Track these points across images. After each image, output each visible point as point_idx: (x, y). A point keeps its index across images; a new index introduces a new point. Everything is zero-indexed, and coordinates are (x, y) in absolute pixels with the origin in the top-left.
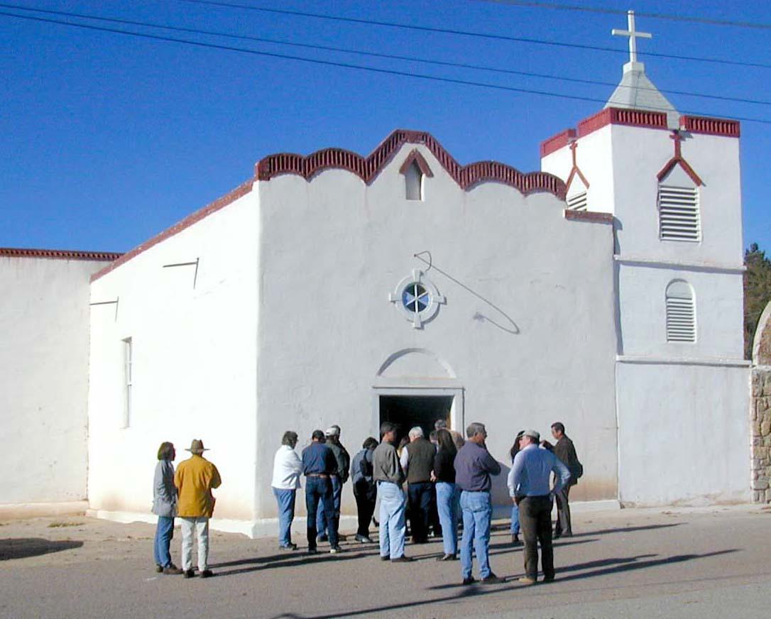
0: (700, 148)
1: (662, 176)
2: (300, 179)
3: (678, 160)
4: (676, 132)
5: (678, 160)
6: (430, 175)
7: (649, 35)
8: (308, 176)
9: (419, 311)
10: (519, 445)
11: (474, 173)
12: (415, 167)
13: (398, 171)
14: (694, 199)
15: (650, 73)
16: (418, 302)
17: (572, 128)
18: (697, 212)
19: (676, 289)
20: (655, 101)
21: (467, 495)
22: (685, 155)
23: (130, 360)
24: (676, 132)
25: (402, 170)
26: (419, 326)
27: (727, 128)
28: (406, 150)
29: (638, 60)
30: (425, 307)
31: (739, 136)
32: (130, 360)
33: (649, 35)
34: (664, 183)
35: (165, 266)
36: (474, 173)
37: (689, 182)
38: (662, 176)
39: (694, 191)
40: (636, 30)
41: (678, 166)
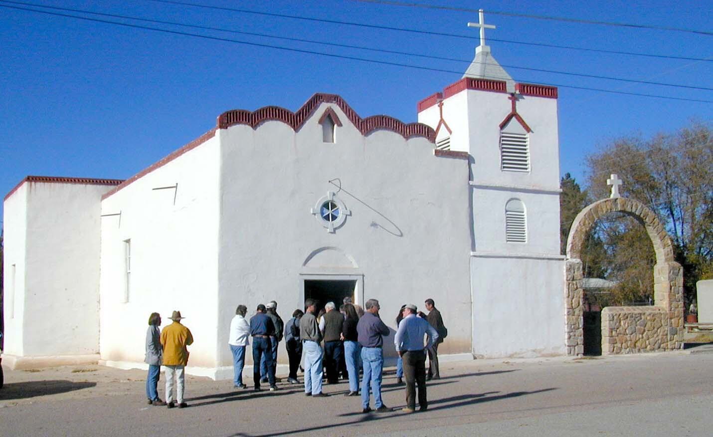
0: (529, 106)
1: (503, 126)
2: (248, 128)
3: (514, 114)
4: (512, 95)
5: (514, 114)
6: (340, 125)
7: (494, 27)
8: (254, 126)
11: (371, 123)
12: (330, 119)
14: (525, 142)
15: (494, 53)
20: (498, 73)
22: (519, 111)
23: (129, 255)
24: (512, 95)
27: (549, 92)
28: (323, 107)
31: (557, 98)
32: (129, 255)
33: (494, 27)
34: (505, 130)
35: (154, 189)
36: (371, 123)
37: (522, 130)
38: (503, 126)
41: (514, 119)
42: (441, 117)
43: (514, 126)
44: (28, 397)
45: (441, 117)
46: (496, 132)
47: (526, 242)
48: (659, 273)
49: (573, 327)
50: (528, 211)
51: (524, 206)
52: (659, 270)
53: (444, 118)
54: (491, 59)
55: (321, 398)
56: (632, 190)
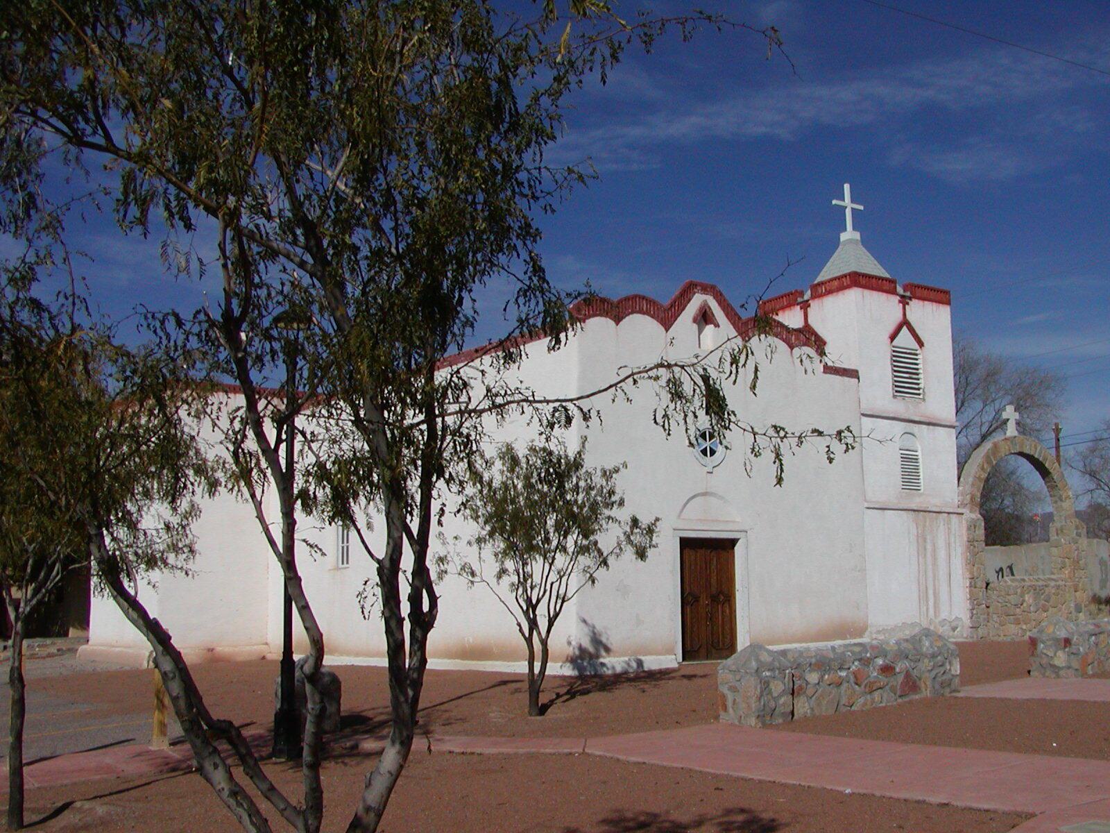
0: (920, 312)
1: (893, 338)
3: (905, 323)
4: (903, 297)
5: (905, 323)
6: (717, 325)
7: (861, 208)
9: (711, 456)
10: (1037, 460)
13: (691, 320)
14: (917, 359)
15: (865, 242)
16: (710, 448)
17: (514, 366)
18: (920, 371)
19: (909, 442)
20: (872, 267)
21: (1079, 461)
22: (910, 317)
23: (347, 542)
24: (903, 297)
25: (695, 321)
26: (444, 574)
27: (939, 296)
28: (697, 300)
29: (854, 228)
30: (715, 452)
31: (948, 303)
32: (347, 542)
34: (896, 342)
38: (893, 338)
39: (918, 352)
40: (852, 202)
41: (905, 329)
42: (904, 314)
43: (905, 338)
44: (833, 253)
45: (904, 314)
46: (885, 351)
47: (922, 491)
48: (1057, 534)
49: (975, 602)
50: (922, 450)
51: (919, 446)
52: (1057, 530)
53: (810, 321)
54: (862, 251)
55: (753, 370)
56: (461, 191)
